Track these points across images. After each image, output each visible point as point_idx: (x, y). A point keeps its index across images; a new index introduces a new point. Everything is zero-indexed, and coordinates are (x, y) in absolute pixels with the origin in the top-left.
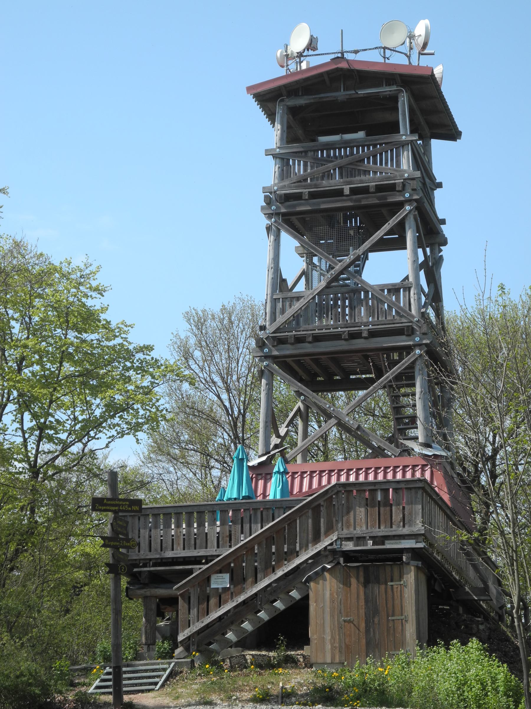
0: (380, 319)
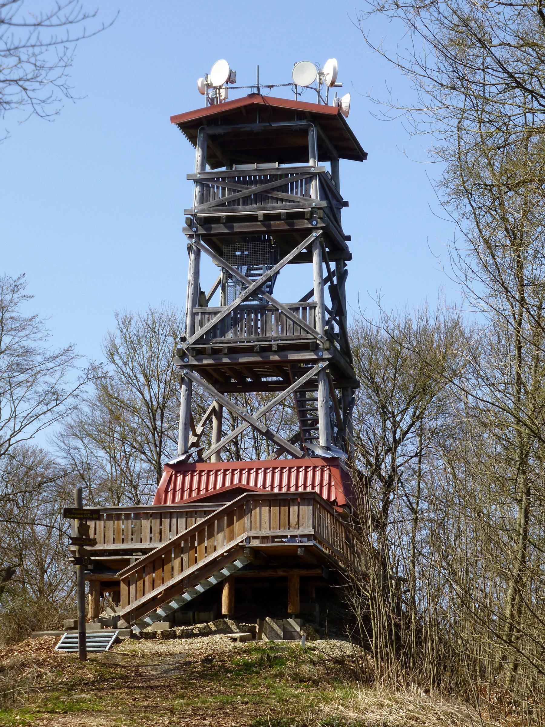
0: (288, 334)
